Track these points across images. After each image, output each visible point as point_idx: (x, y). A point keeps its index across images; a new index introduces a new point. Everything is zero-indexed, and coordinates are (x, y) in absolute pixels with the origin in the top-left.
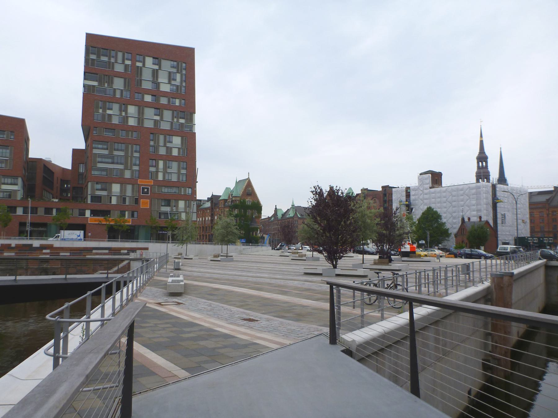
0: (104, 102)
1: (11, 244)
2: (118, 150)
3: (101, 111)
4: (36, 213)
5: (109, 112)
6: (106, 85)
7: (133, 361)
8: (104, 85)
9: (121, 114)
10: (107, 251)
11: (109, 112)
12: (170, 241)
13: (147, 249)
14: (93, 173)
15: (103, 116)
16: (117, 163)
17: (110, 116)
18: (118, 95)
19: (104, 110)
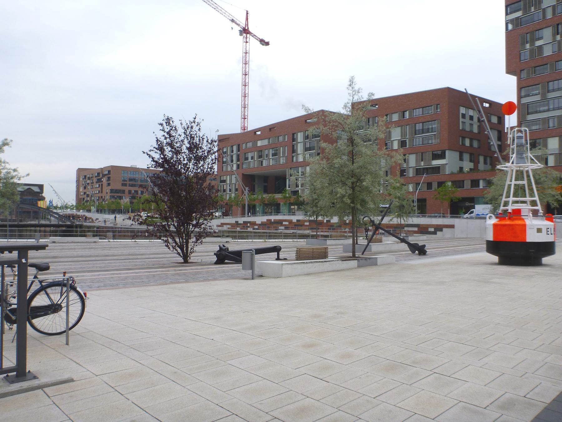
0: (532, 33)
1: (292, 220)
2: (554, 90)
3: (528, 46)
4: (463, 187)
5: (538, 43)
6: (533, 9)
7: (27, 352)
8: (530, 10)
9: (554, 40)
10: (416, 229)
11: (538, 43)
12: (99, 213)
13: (452, 226)
14: (299, 134)
15: (532, 51)
16: (554, 109)
17: (540, 47)
18: (549, 15)
19: (532, 43)
